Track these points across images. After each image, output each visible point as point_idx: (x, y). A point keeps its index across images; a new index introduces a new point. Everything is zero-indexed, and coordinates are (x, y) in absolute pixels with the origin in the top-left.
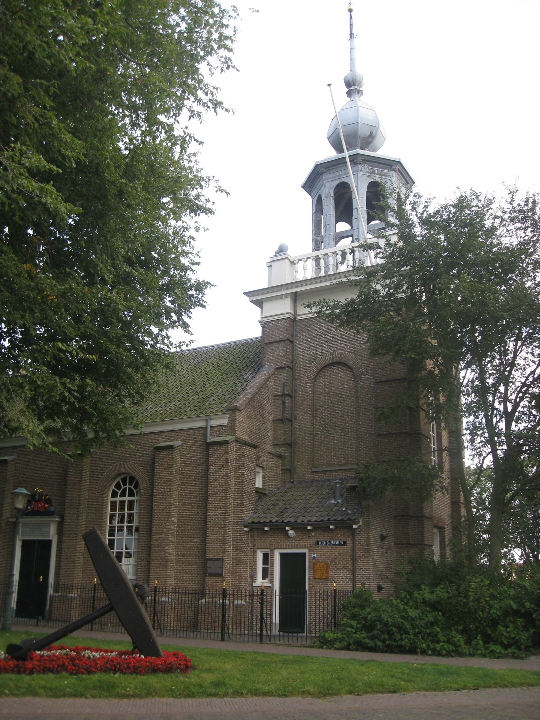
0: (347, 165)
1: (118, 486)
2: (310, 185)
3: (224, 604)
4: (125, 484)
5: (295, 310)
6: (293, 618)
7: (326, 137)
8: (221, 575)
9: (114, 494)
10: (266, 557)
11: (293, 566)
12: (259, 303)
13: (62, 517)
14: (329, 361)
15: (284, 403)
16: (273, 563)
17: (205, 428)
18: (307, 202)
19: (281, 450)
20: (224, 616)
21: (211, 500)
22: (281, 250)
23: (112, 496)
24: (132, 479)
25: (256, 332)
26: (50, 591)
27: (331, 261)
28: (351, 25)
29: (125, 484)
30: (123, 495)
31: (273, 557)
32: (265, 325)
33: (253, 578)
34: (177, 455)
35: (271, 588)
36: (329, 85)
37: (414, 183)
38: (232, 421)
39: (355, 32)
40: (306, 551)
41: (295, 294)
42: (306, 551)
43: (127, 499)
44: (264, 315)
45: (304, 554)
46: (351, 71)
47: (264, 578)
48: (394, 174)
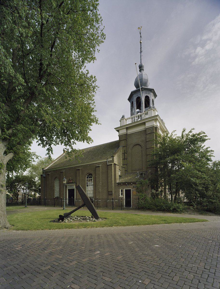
0: (140, 91)
1: (88, 176)
2: (130, 99)
3: (113, 201)
4: (89, 176)
5: (127, 132)
6: (128, 204)
7: (134, 84)
8: (112, 195)
9: (87, 178)
10: (122, 190)
11: (128, 193)
12: (118, 131)
13: (76, 183)
14: (135, 144)
15: (125, 155)
16: (123, 192)
17: (107, 161)
18: (129, 104)
19: (124, 166)
20: (113, 204)
21: (109, 178)
22: (123, 117)
23: (87, 176)
24: (91, 174)
25: (117, 139)
26: (75, 200)
27: (136, 118)
28: (141, 59)
29: (89, 176)
30: (89, 178)
31: (123, 190)
32: (120, 136)
33: (119, 195)
34: (100, 168)
35: (123, 197)
36: (136, 64)
37: (157, 96)
38: (113, 159)
39: (142, 50)
40: (131, 189)
41: (127, 128)
42: (131, 189)
43: (90, 179)
44: (120, 133)
45: (131, 189)
46: (141, 63)
47: (121, 195)
48: (152, 93)
